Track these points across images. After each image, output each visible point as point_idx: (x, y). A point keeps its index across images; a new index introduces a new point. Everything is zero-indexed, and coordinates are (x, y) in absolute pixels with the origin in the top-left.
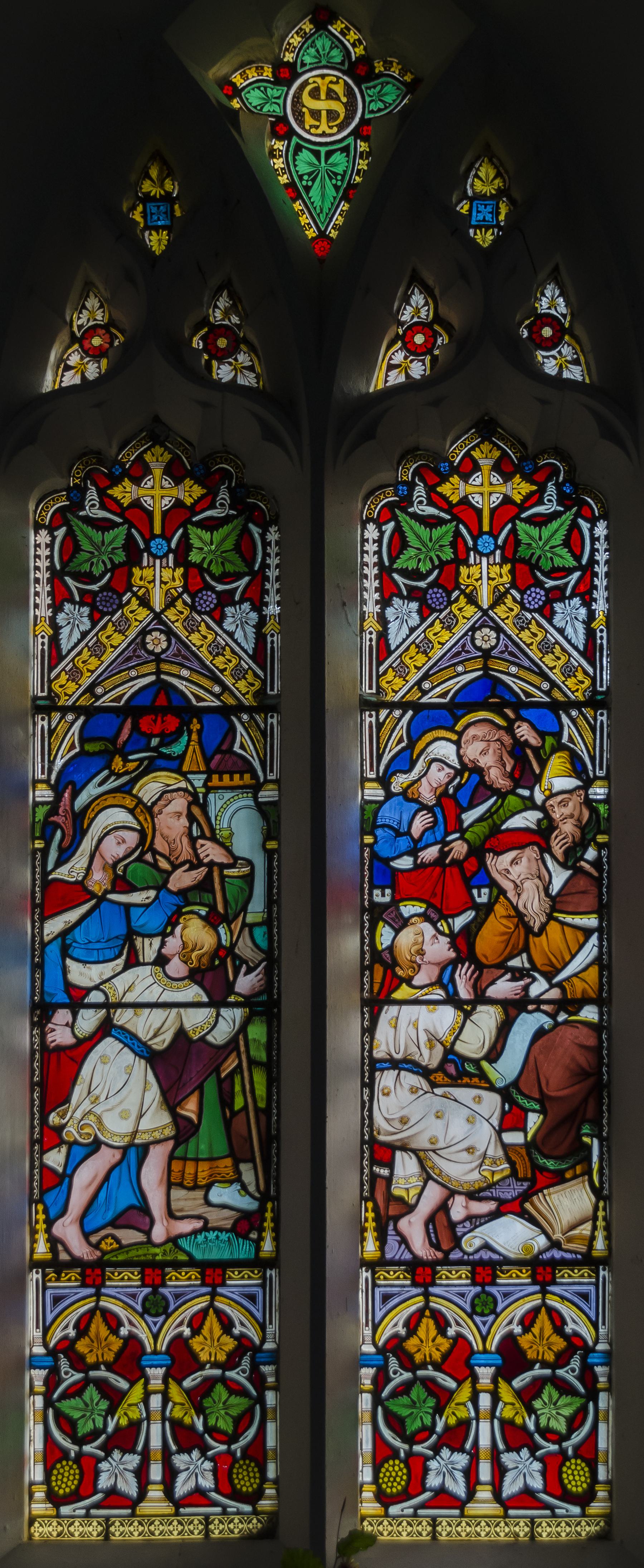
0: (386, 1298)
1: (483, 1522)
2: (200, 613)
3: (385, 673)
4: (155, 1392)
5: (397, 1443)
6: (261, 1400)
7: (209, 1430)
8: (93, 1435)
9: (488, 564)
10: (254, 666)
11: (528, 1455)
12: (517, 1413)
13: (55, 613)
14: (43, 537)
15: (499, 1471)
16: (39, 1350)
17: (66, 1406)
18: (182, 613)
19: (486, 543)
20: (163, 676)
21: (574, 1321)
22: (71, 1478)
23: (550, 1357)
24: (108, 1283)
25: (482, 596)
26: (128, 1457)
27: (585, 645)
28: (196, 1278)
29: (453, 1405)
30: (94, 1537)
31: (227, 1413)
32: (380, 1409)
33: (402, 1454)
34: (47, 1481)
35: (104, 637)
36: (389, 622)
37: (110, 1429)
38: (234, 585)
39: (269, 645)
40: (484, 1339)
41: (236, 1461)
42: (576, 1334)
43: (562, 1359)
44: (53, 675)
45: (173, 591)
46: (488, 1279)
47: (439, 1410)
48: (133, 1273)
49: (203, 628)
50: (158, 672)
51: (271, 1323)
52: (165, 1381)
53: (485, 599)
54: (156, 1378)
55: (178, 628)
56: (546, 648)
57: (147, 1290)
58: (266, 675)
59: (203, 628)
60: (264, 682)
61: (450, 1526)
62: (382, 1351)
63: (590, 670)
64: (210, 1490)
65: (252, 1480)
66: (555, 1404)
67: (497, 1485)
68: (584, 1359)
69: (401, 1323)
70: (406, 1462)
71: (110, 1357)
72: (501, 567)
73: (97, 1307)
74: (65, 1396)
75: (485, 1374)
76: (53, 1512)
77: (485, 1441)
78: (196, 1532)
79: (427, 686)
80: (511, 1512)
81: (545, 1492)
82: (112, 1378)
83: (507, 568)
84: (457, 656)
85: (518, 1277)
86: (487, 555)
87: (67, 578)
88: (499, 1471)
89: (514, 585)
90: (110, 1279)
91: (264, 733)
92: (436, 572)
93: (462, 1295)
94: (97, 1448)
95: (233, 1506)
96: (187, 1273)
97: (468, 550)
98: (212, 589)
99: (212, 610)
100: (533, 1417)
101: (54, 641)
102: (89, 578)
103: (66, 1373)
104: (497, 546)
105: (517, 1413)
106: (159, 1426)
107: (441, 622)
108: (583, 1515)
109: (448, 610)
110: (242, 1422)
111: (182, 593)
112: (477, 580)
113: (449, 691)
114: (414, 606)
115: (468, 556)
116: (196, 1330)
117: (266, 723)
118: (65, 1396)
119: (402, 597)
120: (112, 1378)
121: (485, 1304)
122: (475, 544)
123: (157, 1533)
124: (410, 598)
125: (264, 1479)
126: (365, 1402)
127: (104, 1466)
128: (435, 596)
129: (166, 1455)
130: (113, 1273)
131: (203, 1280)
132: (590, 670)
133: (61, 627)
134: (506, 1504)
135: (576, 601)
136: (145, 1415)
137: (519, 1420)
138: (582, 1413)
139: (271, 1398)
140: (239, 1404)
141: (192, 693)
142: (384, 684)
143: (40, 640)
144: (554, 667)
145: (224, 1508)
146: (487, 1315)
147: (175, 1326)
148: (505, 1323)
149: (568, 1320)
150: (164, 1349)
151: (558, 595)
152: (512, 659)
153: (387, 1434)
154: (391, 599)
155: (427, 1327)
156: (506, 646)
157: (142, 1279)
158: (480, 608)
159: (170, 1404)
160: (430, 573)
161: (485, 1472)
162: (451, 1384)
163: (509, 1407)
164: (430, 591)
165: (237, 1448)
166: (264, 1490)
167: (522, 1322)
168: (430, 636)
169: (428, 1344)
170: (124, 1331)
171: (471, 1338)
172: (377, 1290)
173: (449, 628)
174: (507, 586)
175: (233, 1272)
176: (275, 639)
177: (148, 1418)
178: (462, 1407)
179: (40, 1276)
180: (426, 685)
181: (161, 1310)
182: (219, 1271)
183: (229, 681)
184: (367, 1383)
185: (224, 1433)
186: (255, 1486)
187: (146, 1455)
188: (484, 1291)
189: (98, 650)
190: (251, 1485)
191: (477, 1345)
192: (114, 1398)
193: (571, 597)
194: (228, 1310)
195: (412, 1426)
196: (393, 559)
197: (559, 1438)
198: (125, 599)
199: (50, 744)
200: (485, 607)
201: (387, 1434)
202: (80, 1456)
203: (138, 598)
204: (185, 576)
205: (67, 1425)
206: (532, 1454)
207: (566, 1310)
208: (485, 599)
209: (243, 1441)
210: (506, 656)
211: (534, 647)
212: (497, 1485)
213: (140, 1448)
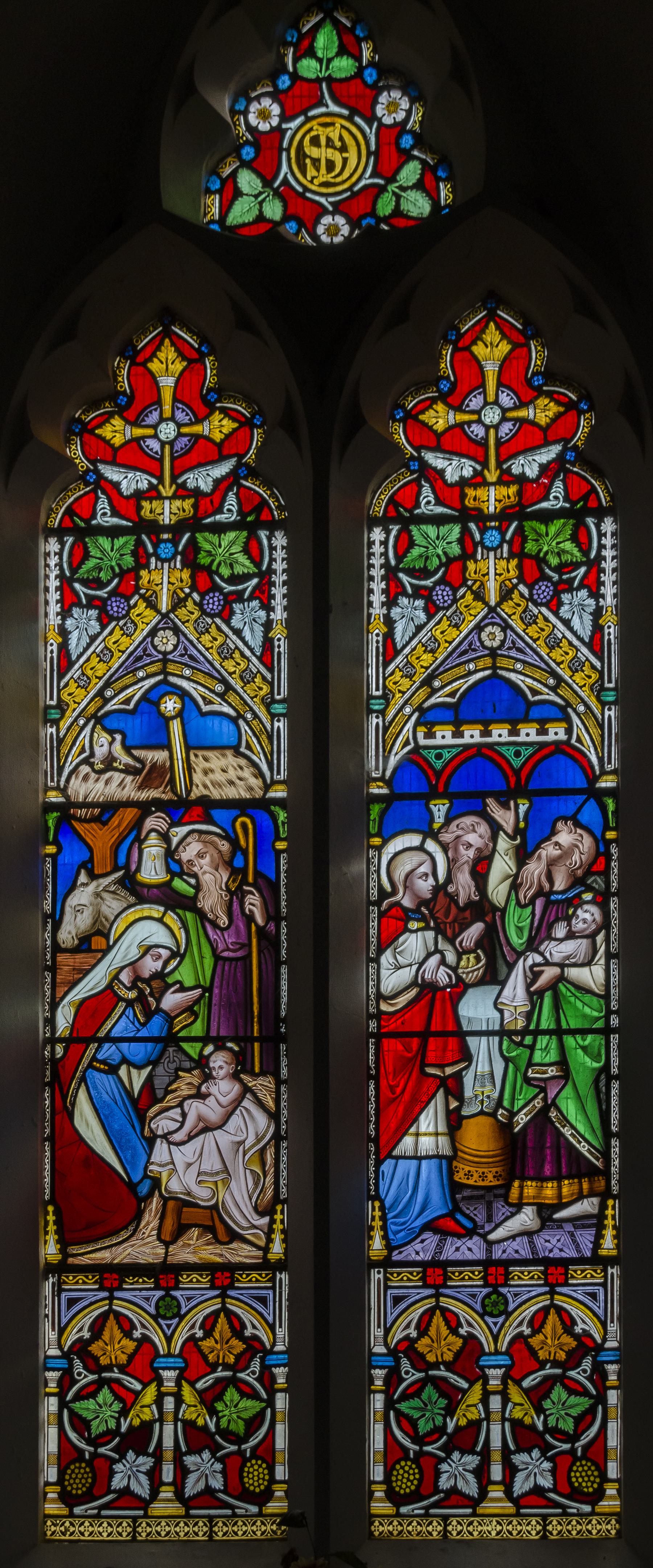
0: (71, 1302)
1: (494, 1522)
2: (536, 604)
3: (392, 673)
4: (495, 1393)
5: (407, 1442)
6: (271, 1403)
7: (220, 1431)
8: (108, 1435)
9: (496, 558)
10: (262, 669)
11: (539, 1455)
12: (526, 1414)
13: (64, 619)
14: (53, 545)
15: (510, 1470)
16: (54, 1352)
17: (404, 1407)
18: (519, 605)
19: (166, 550)
20: (500, 672)
21: (584, 1322)
22: (400, 1477)
23: (562, 1356)
24: (570, 1282)
25: (489, 591)
26: (141, 1459)
27: (592, 638)
28: (539, 1278)
29: (138, 1407)
30: (534, 1536)
31: (567, 1414)
32: (66, 1411)
33: (87, 1456)
34: (60, 1482)
35: (438, 632)
36: (395, 622)
37: (123, 1429)
38: (240, 587)
39: (606, 638)
40: (496, 1338)
41: (246, 1460)
42: (587, 1334)
43: (573, 1359)
44: (62, 684)
45: (507, 582)
46: (172, 1284)
47: (450, 1411)
48: (595, 1271)
49: (213, 630)
50: (494, 667)
51: (280, 1326)
52: (179, 1385)
53: (164, 604)
54: (169, 1380)
55: (189, 630)
56: (226, 653)
57: (159, 1294)
58: (273, 678)
59: (213, 630)
60: (601, 673)
61: (401, 1525)
62: (66, 1355)
63: (598, 664)
64: (220, 1491)
65: (261, 1481)
66: (236, 1406)
67: (179, 1484)
68: (263, 1360)
69: (86, 1328)
70: (89, 1463)
71: (449, 1357)
72: (508, 562)
73: (111, 1310)
74: (78, 1397)
75: (495, 1377)
76: (65, 1511)
77: (496, 1442)
78: (201, 1534)
79: (109, 693)
80: (193, 1512)
81: (224, 1492)
82: (453, 1378)
83: (514, 563)
84: (464, 651)
85: (84, 1283)
86: (494, 549)
87: (401, 575)
88: (182, 1472)
89: (521, 579)
90: (573, 1277)
91: (270, 738)
92: (116, 581)
93: (474, 1296)
94: (111, 1450)
95: (575, 1507)
96: (74, 1277)
97: (475, 545)
98: (220, 590)
99: (221, 612)
100: (542, 1417)
101: (63, 648)
102: (98, 584)
103: (407, 1373)
104: (503, 540)
105: (526, 1414)
106: (172, 1427)
107: (122, 629)
108: (260, 1514)
109: (454, 607)
110: (583, 1421)
111: (517, 584)
112: (484, 575)
113: (458, 690)
114: (93, 613)
115: (476, 551)
116: (208, 1332)
117: (272, 725)
118: (78, 1397)
119: (408, 596)
120: (453, 1378)
121: (168, 1307)
122: (482, 539)
123: (240, 1533)
124: (90, 605)
125: (604, 1478)
126: (378, 1402)
127: (119, 1467)
128: (442, 595)
129: (506, 1453)
130: (241, 1275)
131: (546, 1280)
132: (598, 664)
133: (70, 632)
134: (188, 1503)
135: (584, 593)
136: (483, 1416)
137: (200, 1422)
138: (590, 1412)
139: (613, 1397)
140: (580, 1404)
141: (528, 687)
142: (390, 685)
143: (49, 648)
144: (562, 662)
145: (232, 1507)
146: (171, 1318)
147: (517, 1324)
148: (515, 1324)
149: (579, 1321)
150: (177, 1351)
151: (568, 586)
152: (520, 656)
153: (73, 1436)
154: (70, 610)
155: (112, 1329)
156: (513, 642)
157: (212, 1281)
158: (486, 604)
159: (510, 1405)
160: (109, 582)
161: (168, 1473)
162: (138, 1386)
163: (518, 1408)
164: (438, 588)
165: (247, 1446)
166: (605, 1490)
167: (531, 1324)
168: (110, 645)
169: (115, 1348)
170: (137, 1334)
171: (483, 1340)
172: (389, 1292)
173: (457, 626)
174: (515, 581)
175: (67, 1277)
176: (612, 630)
177: (488, 1418)
178: (473, 1409)
179: (381, 1276)
180: (109, 693)
181: (488, 1309)
182: (561, 1270)
183: (566, 675)
184: (52, 1387)
185: (236, 1435)
186: (262, 1487)
187: (158, 1455)
188: (168, 1295)
189: (105, 655)
190: (259, 1485)
191: (162, 1348)
192: (453, 1398)
193: (578, 589)
194: (239, 1311)
195: (424, 1427)
196: (400, 557)
197: (239, 1440)
198: (132, 602)
199: (384, 741)
200: (493, 603)
201: (73, 1436)
202: (420, 1454)
203: (473, 592)
204: (519, 567)
205: (408, 1424)
206: (543, 1454)
207: (576, 1311)
208: (164, 604)
209: (253, 1442)
210: (513, 653)
211: (214, 651)
212: (179, 1484)
213: (151, 1449)
